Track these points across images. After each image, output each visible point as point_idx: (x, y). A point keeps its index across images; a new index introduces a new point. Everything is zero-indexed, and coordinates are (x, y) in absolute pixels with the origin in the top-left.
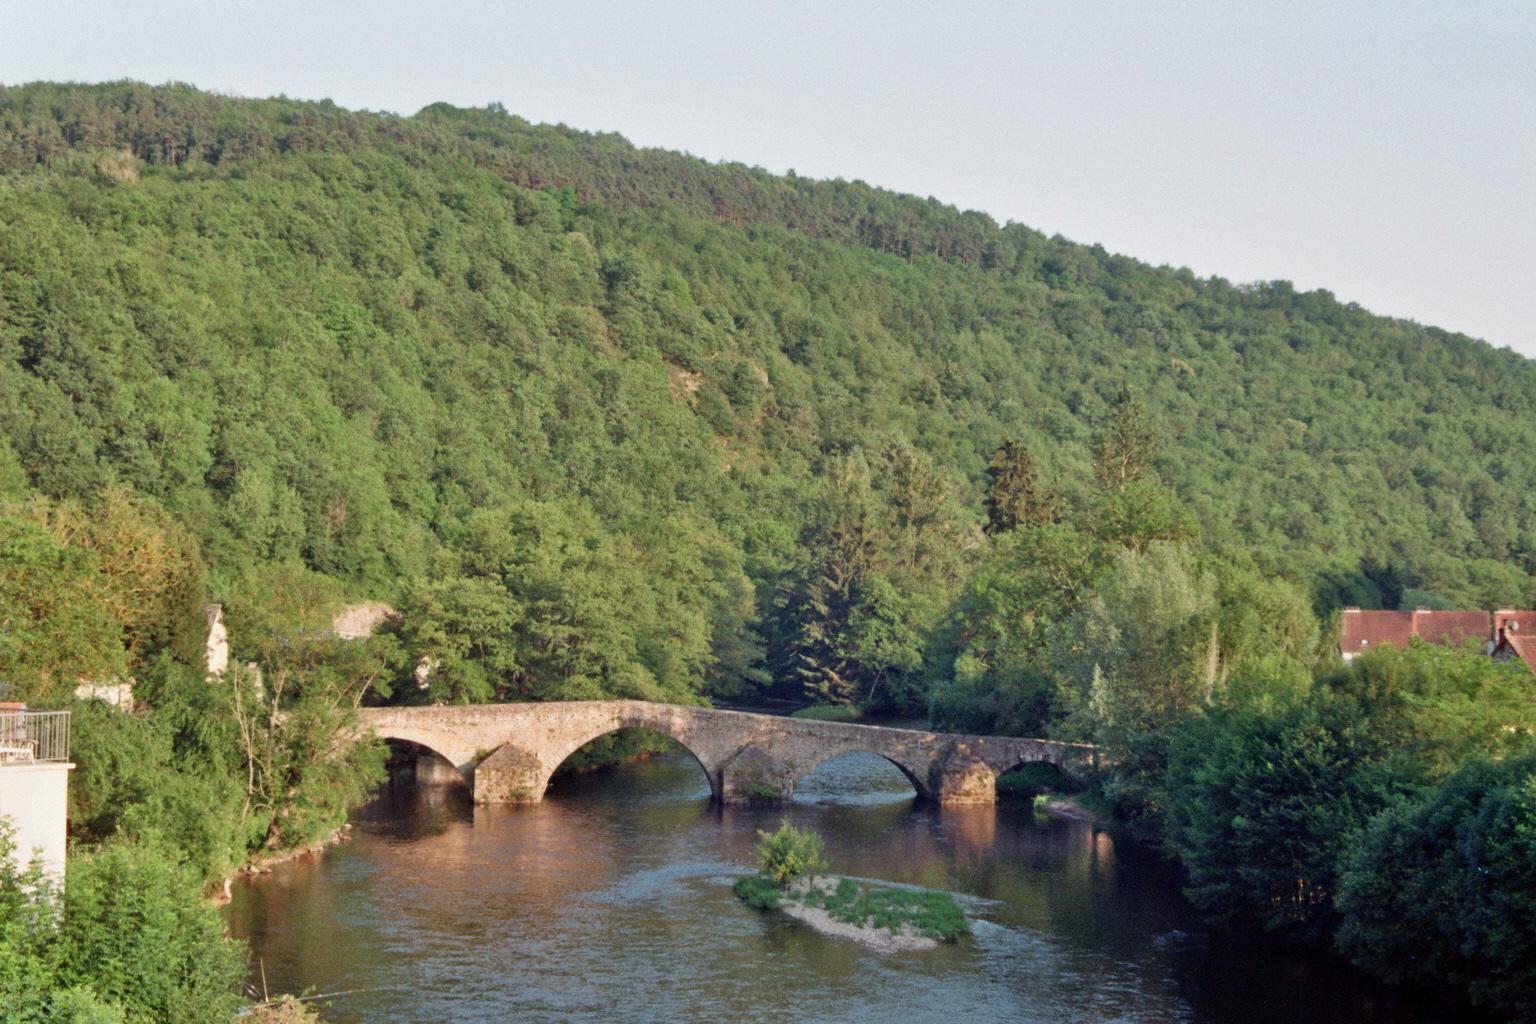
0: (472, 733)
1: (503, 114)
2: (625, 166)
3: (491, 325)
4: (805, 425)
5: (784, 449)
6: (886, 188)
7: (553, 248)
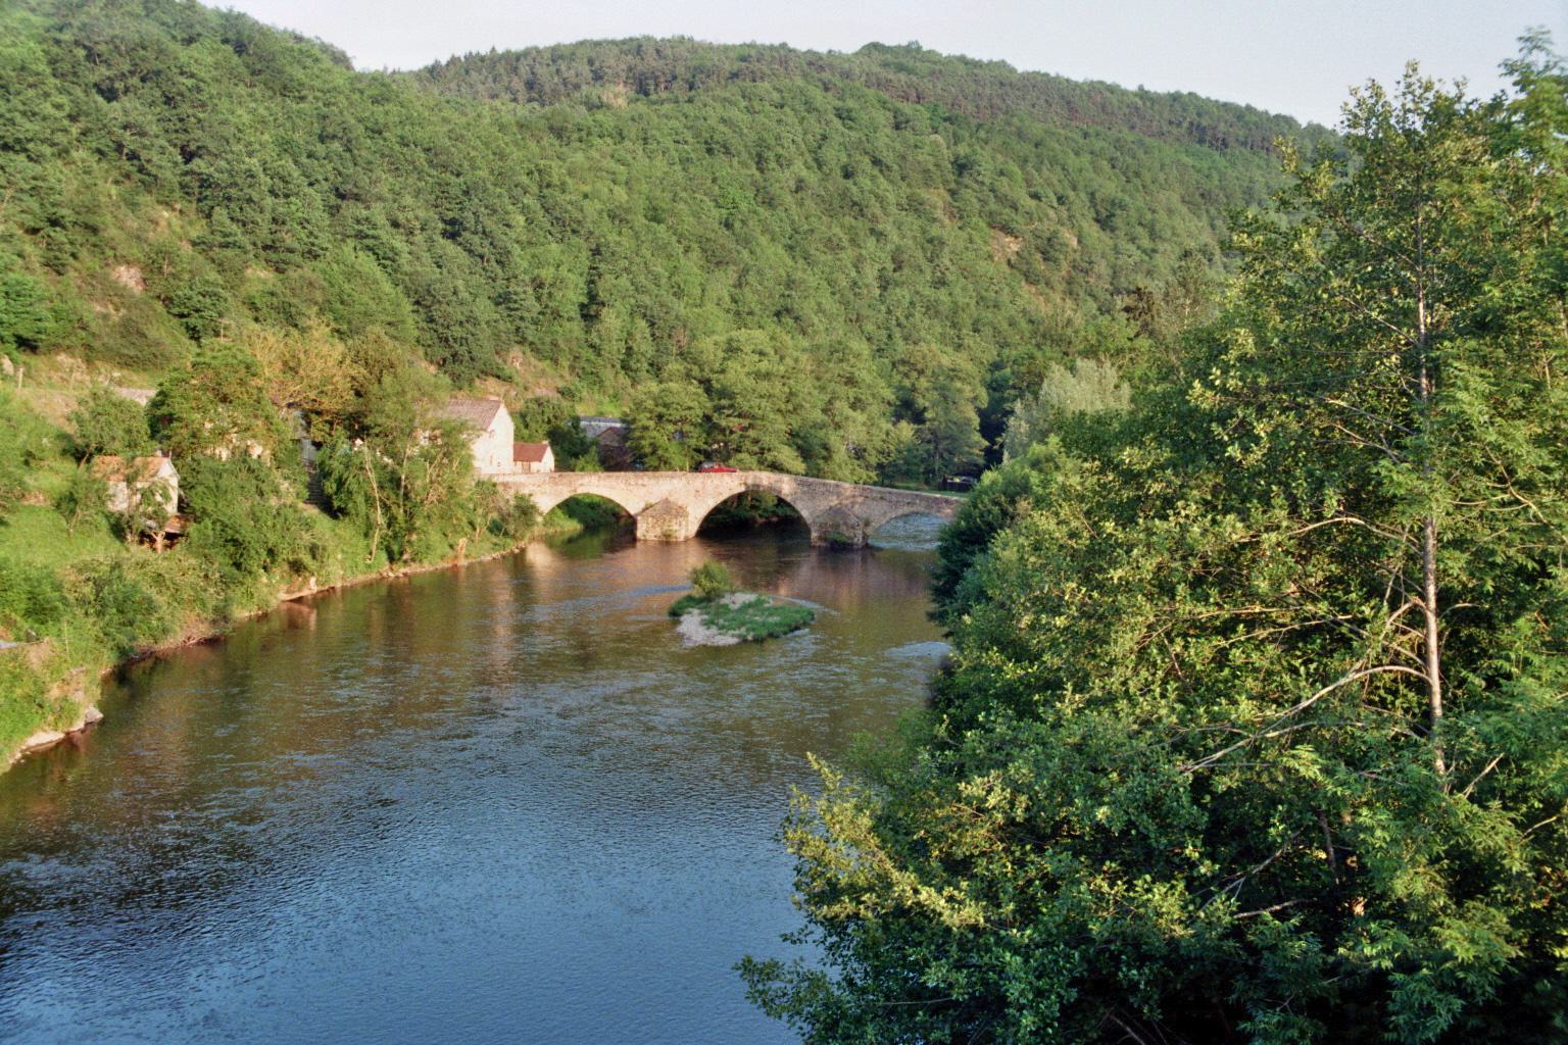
0: (643, 491)
1: (919, 48)
2: (1002, 84)
3: (855, 204)
4: (1099, 277)
5: (1082, 294)
6: (1213, 98)
7: (916, 146)
